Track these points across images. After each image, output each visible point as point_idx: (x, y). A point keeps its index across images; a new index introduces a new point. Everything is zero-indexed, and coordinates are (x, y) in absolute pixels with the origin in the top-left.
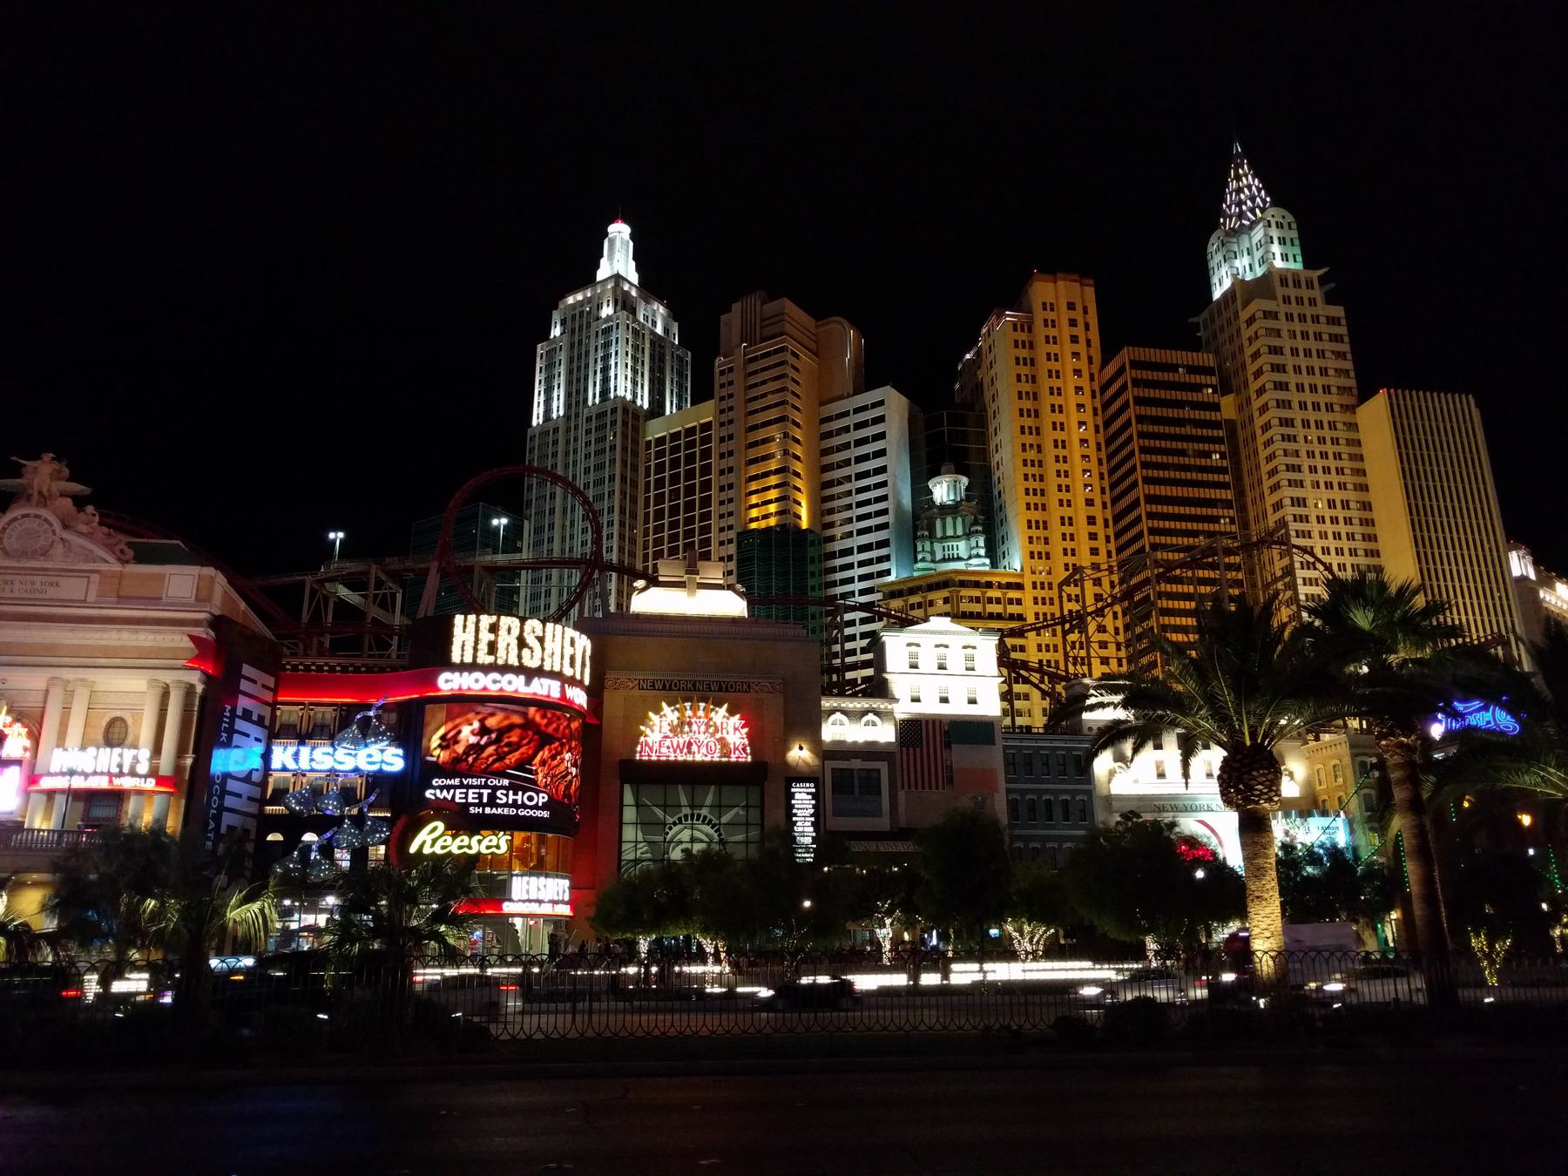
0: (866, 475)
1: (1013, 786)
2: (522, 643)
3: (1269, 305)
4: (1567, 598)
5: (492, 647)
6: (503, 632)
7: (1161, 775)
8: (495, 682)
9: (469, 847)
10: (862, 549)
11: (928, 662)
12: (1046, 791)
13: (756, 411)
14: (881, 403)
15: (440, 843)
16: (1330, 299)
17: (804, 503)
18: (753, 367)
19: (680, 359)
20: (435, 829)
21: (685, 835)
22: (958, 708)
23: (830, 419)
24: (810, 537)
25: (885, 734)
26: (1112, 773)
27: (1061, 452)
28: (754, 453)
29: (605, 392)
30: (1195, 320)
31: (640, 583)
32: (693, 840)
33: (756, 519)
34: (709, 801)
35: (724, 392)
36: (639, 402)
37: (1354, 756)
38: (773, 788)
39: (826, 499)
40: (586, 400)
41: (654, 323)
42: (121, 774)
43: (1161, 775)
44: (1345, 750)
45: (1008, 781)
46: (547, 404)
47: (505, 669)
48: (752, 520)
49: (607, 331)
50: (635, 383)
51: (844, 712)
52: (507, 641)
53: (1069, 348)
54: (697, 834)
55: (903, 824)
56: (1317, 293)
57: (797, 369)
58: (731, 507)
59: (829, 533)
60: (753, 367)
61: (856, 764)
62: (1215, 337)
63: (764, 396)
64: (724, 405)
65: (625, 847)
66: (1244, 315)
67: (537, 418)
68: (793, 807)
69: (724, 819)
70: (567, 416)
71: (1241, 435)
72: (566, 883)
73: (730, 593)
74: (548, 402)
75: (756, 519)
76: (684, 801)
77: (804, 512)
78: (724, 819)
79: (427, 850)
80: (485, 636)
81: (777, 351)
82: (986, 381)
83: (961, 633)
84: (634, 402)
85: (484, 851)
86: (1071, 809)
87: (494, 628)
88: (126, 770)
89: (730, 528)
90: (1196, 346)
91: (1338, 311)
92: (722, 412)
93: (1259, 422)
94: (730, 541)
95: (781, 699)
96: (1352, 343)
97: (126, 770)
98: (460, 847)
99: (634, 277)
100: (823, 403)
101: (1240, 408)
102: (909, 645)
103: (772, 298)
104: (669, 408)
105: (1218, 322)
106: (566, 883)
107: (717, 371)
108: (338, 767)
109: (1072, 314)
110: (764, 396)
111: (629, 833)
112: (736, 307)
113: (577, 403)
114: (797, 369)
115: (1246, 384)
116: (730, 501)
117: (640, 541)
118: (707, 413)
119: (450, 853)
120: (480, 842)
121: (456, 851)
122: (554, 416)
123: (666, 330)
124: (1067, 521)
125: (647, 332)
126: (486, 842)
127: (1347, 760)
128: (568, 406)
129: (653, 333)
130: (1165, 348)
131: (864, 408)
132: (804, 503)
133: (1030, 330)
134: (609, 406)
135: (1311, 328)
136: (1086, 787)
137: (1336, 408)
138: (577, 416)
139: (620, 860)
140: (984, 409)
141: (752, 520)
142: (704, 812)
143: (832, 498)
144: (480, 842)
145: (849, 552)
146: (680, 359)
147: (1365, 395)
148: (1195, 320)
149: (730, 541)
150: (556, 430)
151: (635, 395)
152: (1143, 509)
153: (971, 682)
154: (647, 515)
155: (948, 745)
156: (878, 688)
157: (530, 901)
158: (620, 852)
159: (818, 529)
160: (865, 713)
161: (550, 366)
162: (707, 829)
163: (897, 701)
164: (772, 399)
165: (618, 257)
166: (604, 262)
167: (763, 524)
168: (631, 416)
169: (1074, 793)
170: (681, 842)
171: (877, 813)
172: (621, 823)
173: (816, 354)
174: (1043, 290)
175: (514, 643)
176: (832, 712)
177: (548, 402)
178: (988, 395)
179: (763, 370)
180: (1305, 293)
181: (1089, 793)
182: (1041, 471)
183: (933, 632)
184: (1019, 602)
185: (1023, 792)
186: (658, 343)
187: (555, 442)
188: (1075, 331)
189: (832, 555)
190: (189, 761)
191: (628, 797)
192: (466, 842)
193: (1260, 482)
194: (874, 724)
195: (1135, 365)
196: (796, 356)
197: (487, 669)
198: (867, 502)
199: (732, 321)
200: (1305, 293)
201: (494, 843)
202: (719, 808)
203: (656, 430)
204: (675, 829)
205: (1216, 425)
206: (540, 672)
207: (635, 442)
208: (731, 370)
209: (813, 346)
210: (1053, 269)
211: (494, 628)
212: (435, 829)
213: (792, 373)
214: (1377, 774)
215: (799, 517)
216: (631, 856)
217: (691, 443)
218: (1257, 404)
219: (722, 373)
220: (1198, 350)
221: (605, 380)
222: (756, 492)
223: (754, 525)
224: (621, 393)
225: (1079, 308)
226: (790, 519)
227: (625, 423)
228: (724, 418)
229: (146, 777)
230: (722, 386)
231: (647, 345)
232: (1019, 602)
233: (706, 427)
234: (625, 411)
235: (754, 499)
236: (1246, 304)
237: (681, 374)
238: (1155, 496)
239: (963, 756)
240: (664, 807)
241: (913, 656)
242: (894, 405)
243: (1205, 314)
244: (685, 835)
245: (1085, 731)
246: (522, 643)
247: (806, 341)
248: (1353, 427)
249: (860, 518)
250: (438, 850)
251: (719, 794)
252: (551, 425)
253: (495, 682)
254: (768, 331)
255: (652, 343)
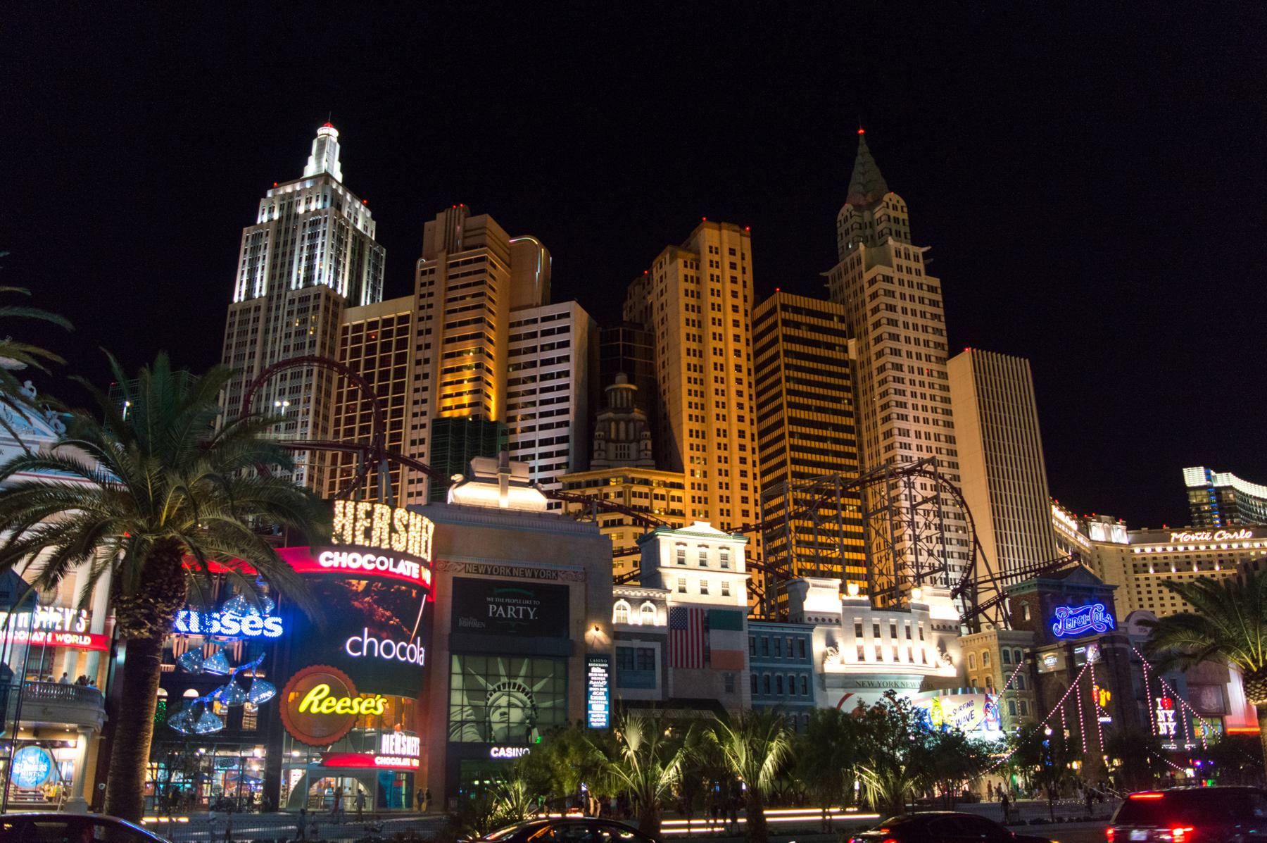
0: (551, 376)
1: (754, 664)
2: (392, 529)
3: (887, 271)
4: (1, 255)
5: (368, 533)
6: (376, 515)
7: (861, 658)
8: (370, 562)
9: (351, 708)
10: (544, 442)
11: (692, 557)
12: (766, 669)
13: (455, 311)
14: (567, 315)
15: (325, 703)
16: (930, 271)
17: (493, 397)
18: (453, 272)
19: (377, 255)
20: (321, 691)
21: (503, 701)
22: (715, 598)
23: (519, 324)
24: (500, 429)
25: (659, 619)
26: (825, 655)
27: (720, 374)
28: (450, 348)
29: (308, 279)
30: (824, 274)
31: (458, 477)
32: (510, 705)
33: (450, 408)
34: (523, 672)
35: (425, 290)
36: (339, 292)
37: (1001, 646)
38: (575, 661)
39: (511, 395)
40: (289, 283)
41: (356, 220)
42: (62, 632)
43: (861, 658)
44: (994, 642)
45: (752, 660)
46: (250, 284)
47: (377, 551)
48: (445, 409)
49: (315, 224)
50: (337, 273)
51: (627, 599)
52: (381, 526)
53: (729, 286)
54: (513, 700)
55: (671, 694)
56: (921, 266)
57: (494, 278)
58: (425, 395)
59: (512, 425)
60: (453, 272)
61: (637, 643)
62: (841, 289)
63: (463, 298)
64: (424, 302)
65: (453, 709)
66: (867, 276)
67: (239, 295)
68: (589, 679)
69: (536, 688)
70: (269, 297)
71: (860, 374)
72: (417, 740)
73: (535, 491)
74: (251, 282)
75: (450, 408)
76: (502, 671)
77: (493, 405)
78: (536, 688)
79: (314, 710)
80: (363, 524)
81: (477, 260)
82: (656, 306)
83: (718, 536)
84: (335, 289)
85: (364, 712)
86: (796, 684)
87: (369, 514)
88: (67, 628)
89: (424, 414)
90: (824, 295)
91: (936, 282)
92: (422, 308)
93: (876, 364)
94: (423, 426)
95: (583, 587)
96: (945, 308)
97: (67, 628)
98: (343, 708)
99: (339, 176)
100: (512, 310)
101: (860, 351)
102: (678, 544)
103: (474, 213)
104: (365, 300)
105: (844, 279)
106: (417, 740)
107: (419, 270)
108: (224, 631)
109: (733, 259)
110: (463, 298)
111: (457, 698)
112: (441, 216)
113: (280, 286)
114: (494, 278)
115: (866, 332)
116: (425, 389)
117: (332, 418)
118: (406, 306)
119: (334, 712)
120: (360, 703)
121: (340, 711)
122: (257, 295)
123: (366, 228)
124: (722, 433)
125: (350, 228)
126: (365, 704)
127: (995, 649)
128: (271, 287)
129: (355, 229)
130: (805, 296)
131: (551, 318)
132: (493, 397)
133: (697, 268)
134: (312, 292)
135: (917, 293)
136: (807, 666)
137: (933, 359)
138: (279, 297)
139: (449, 721)
140: (652, 329)
141: (445, 409)
142: (519, 681)
143: (516, 394)
144: (360, 703)
145: (531, 444)
146: (377, 255)
147: (954, 351)
148: (824, 274)
149: (423, 426)
150: (258, 309)
151: (336, 283)
152: (787, 428)
153: (726, 577)
154: (340, 395)
155: (706, 630)
156: (650, 576)
157: (395, 756)
158: (449, 714)
159: (503, 421)
160: (643, 600)
161: (255, 249)
162: (521, 696)
163: (670, 591)
164: (469, 302)
165: (326, 156)
166: (312, 161)
167: (456, 413)
168: (332, 304)
169: (798, 671)
170: (500, 707)
171: (651, 685)
172: (450, 690)
173: (509, 266)
174: (710, 236)
175: (387, 529)
176: (618, 598)
177: (251, 282)
178: (657, 318)
179: (464, 275)
180: (914, 265)
181: (810, 671)
182: (703, 388)
183: (698, 534)
184: (680, 500)
185: (761, 670)
186: (359, 238)
187: (256, 320)
188: (735, 273)
189: (515, 446)
190: (113, 622)
191: (456, 667)
192: (348, 704)
193: (874, 413)
194: (651, 610)
195: (785, 308)
196: (494, 267)
197: (363, 550)
198: (550, 402)
199: (435, 230)
200: (914, 265)
201: (373, 705)
202: (531, 678)
203: (353, 318)
204: (495, 695)
205: (845, 363)
206: (405, 556)
207: (334, 326)
208: (432, 271)
209: (507, 258)
210: (718, 219)
211: (369, 514)
212: (321, 691)
213: (490, 281)
214: (1029, 661)
215: (488, 409)
216: (458, 718)
217: (394, 331)
218: (874, 349)
219: (424, 273)
220: (825, 299)
221: (310, 268)
222: (451, 383)
223: (447, 414)
224: (325, 281)
225: (738, 254)
226: (481, 411)
227: (326, 309)
228: (423, 313)
229: (83, 634)
230: (423, 285)
231: (350, 240)
232: (680, 500)
233: (404, 319)
234: (328, 298)
235: (448, 390)
236: (868, 268)
237: (376, 268)
238: (796, 419)
239: (718, 639)
240: (486, 676)
241: (681, 553)
242: (576, 317)
243: (834, 270)
244: (503, 701)
245: (806, 621)
246: (392, 529)
247: (501, 253)
248: (944, 375)
249: (543, 415)
250: (324, 709)
251: (531, 668)
252: (253, 304)
253: (370, 562)
254: (469, 242)
255: (354, 238)
